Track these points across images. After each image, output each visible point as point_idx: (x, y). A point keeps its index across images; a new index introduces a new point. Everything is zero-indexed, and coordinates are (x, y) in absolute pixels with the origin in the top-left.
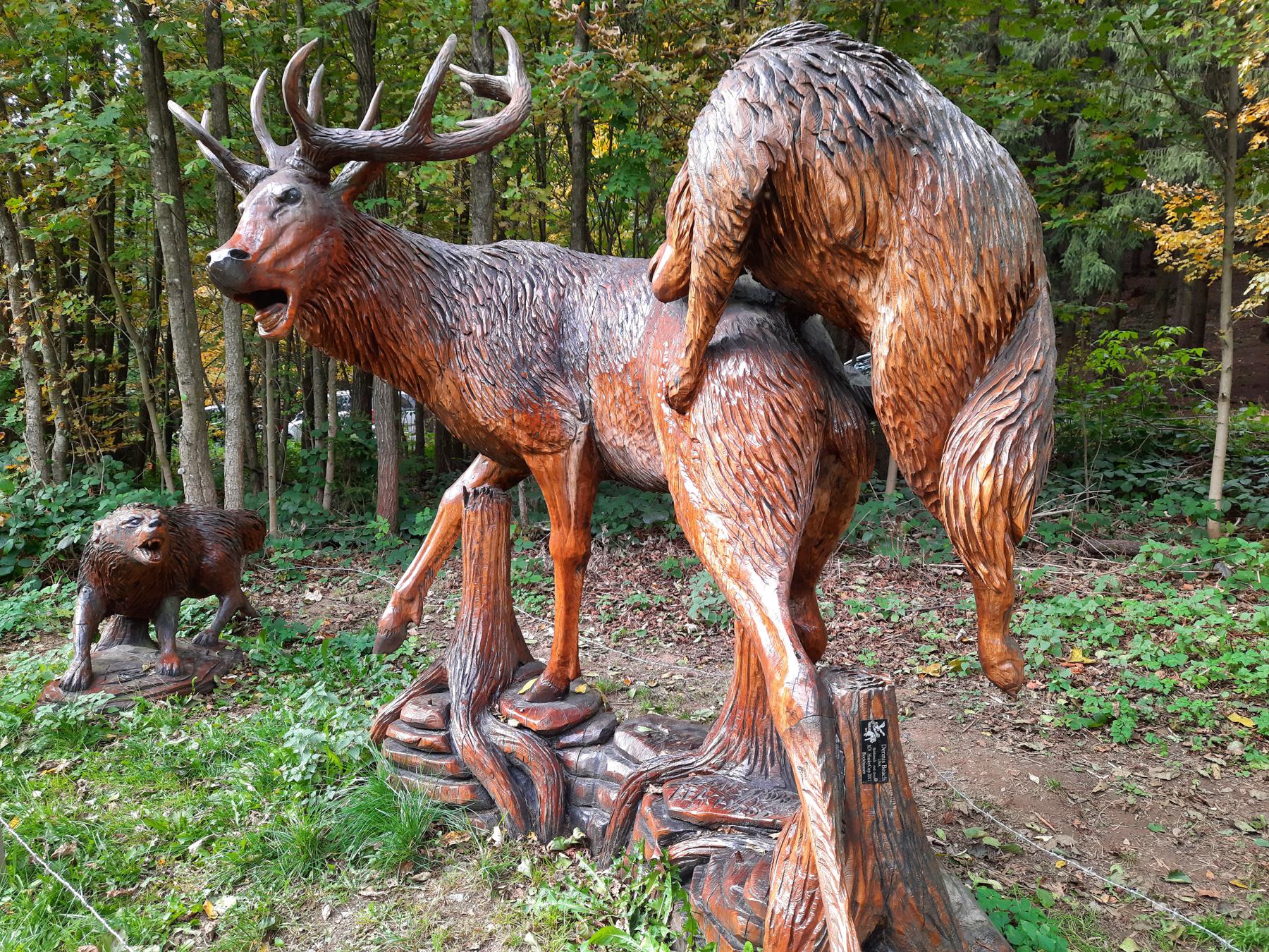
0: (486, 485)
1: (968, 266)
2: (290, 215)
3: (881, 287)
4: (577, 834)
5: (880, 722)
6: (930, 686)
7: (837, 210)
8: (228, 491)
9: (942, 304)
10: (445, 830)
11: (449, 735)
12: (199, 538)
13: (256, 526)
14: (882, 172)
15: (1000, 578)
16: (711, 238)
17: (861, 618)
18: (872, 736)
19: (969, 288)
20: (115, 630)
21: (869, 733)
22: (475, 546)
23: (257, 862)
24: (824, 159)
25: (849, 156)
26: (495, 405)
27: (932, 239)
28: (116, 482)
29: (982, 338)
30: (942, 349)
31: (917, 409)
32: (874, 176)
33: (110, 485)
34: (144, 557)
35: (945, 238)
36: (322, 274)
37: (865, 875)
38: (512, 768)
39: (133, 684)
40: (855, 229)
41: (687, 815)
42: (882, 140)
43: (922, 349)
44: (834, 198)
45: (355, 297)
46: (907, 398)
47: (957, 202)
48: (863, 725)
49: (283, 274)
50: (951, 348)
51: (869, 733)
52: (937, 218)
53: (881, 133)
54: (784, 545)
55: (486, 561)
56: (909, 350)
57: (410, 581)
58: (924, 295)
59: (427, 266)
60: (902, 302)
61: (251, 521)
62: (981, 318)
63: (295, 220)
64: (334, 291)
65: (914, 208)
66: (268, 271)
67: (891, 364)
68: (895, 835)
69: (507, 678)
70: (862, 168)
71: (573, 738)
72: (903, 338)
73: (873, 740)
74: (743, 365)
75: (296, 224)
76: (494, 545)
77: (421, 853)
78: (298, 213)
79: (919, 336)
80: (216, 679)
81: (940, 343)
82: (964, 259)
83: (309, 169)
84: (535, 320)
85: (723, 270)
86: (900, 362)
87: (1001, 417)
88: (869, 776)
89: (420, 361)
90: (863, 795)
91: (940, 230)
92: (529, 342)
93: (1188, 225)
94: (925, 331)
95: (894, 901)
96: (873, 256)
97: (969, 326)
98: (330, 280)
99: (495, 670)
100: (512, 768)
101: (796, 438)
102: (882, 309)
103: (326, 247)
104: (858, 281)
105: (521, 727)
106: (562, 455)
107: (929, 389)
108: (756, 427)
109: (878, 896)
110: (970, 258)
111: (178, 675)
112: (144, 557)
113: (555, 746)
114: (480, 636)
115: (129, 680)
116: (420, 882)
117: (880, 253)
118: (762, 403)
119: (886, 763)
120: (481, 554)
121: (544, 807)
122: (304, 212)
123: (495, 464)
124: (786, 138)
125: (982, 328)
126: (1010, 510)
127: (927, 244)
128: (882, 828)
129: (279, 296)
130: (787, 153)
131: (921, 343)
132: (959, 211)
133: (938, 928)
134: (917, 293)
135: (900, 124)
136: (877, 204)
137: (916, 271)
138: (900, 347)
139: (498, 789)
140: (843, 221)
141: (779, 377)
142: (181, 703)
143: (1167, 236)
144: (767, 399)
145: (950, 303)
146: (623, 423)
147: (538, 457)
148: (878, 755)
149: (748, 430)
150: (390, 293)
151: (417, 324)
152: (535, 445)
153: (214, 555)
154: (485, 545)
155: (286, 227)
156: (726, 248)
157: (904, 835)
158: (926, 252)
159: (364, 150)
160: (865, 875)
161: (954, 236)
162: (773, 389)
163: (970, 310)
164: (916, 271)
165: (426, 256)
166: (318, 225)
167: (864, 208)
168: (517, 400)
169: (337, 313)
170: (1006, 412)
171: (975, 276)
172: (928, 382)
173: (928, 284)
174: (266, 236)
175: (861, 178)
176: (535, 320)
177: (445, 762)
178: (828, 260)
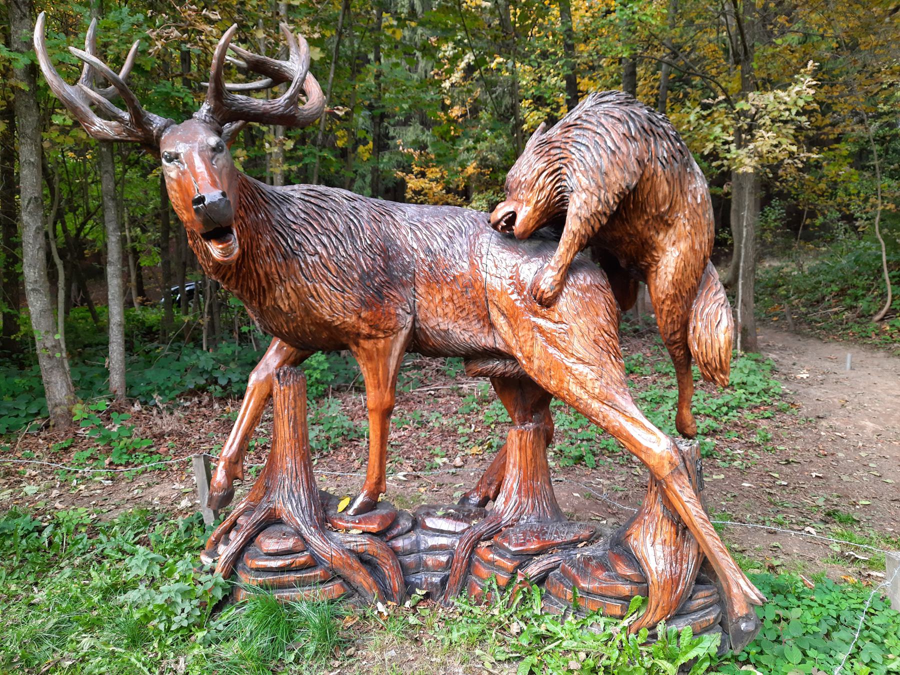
3: (670, 239)
4: (420, 592)
16: (597, 207)
22: (292, 412)
26: (344, 307)
38: (365, 560)
41: (527, 550)
60: (683, 246)
67: (676, 277)
71: (395, 532)
72: (683, 264)
74: (589, 279)
85: (597, 226)
86: (680, 276)
89: (266, 274)
92: (369, 261)
93: (423, 175)
96: (670, 222)
100: (365, 560)
102: (670, 249)
118: (603, 299)
121: (396, 583)
123: (292, 349)
139: (361, 578)
143: (412, 181)
146: (450, 315)
147: (372, 341)
152: (374, 333)
156: (605, 214)
168: (362, 302)
178: (650, 222)
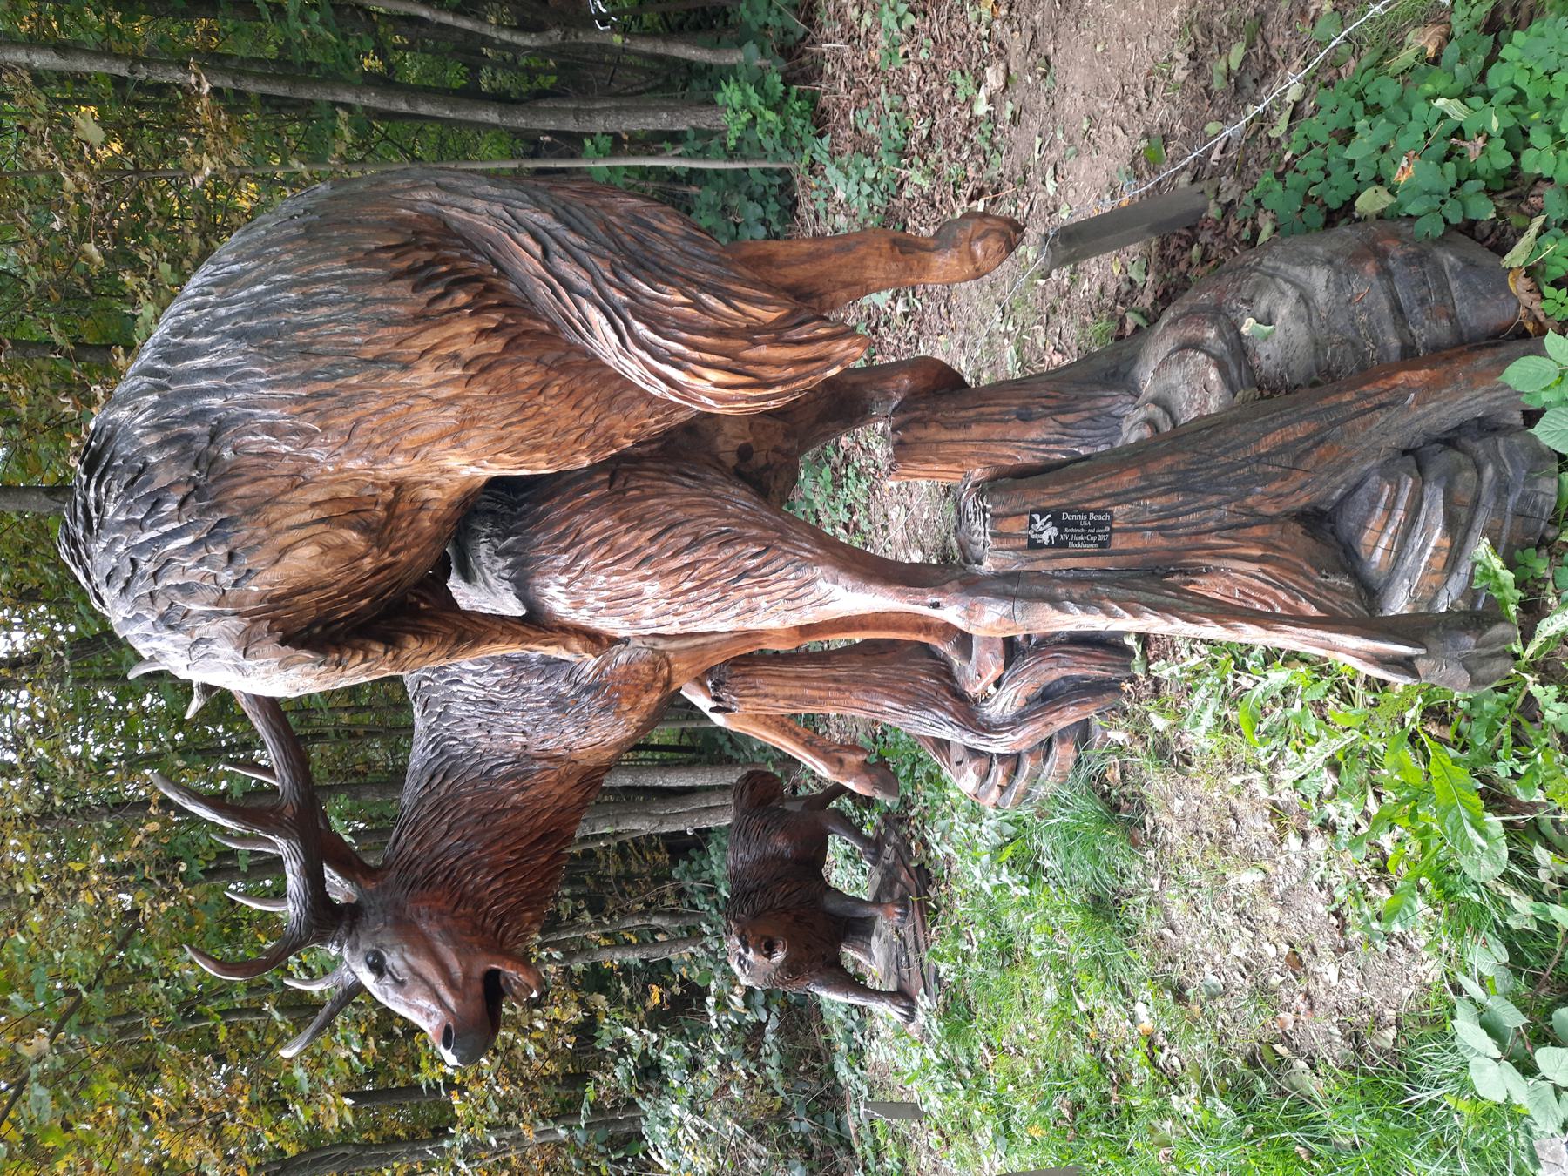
0: (709, 684)
1: (393, 376)
2: (399, 964)
5: (1032, 521)
6: (1010, 8)
7: (329, 558)
8: (714, 782)
9: (451, 412)
10: (1103, 780)
11: (999, 755)
12: (763, 861)
13: (752, 788)
14: (267, 502)
15: (849, 347)
17: (906, 55)
18: (1049, 533)
19: (425, 375)
20: (855, 948)
21: (1045, 538)
22: (781, 703)
23: (1105, 970)
24: (258, 579)
25: (249, 551)
27: (357, 432)
28: (702, 870)
29: (497, 344)
30: (518, 406)
31: (605, 422)
32: (274, 514)
33: (706, 876)
34: (779, 957)
35: (352, 416)
36: (462, 922)
37: (1228, 547)
39: (912, 957)
40: (353, 528)
42: (219, 506)
43: (519, 431)
44: (312, 564)
45: (488, 874)
46: (590, 437)
47: (298, 401)
48: (1034, 545)
49: (467, 976)
50: (518, 393)
51: (1045, 538)
52: (324, 428)
53: (209, 508)
54: (790, 568)
55: (800, 692)
56: (522, 447)
57: (820, 764)
58: (441, 437)
59: (445, 778)
61: (746, 794)
62: (468, 350)
63: (403, 958)
64: (482, 901)
65: (313, 455)
66: (464, 999)
68: (1184, 504)
69: (939, 672)
70: (262, 532)
72: (506, 457)
73: (1054, 532)
75: (407, 956)
76: (780, 681)
77: (1121, 812)
78: (395, 954)
79: (500, 439)
80: (915, 865)
81: (509, 410)
82: (382, 387)
83: (341, 933)
84: (503, 687)
87: (614, 338)
88: (1101, 538)
90: (1124, 547)
91: (343, 422)
94: (493, 431)
95: (1270, 509)
96: (389, 495)
97: (481, 367)
98: (469, 909)
99: (929, 687)
100: (1048, 698)
101: (650, 534)
103: (431, 918)
104: (427, 501)
105: (997, 684)
106: (672, 656)
107: (577, 412)
108: (635, 586)
109: (1258, 531)
110: (381, 375)
111: (906, 908)
112: (779, 957)
113: (1025, 645)
114: (888, 703)
115: (908, 960)
116: (1155, 830)
117: (384, 488)
118: (602, 578)
119: (1087, 512)
120: (790, 698)
122: (392, 947)
124: (234, 624)
125: (483, 346)
126: (752, 334)
127: (364, 440)
128: (1172, 521)
129: (492, 977)
130: (254, 622)
131: (511, 433)
132: (311, 396)
133: (1317, 445)
134: (438, 447)
135: (191, 479)
136: (314, 505)
137: (406, 451)
138: (518, 459)
139: (1070, 715)
140: (345, 545)
141: (565, 550)
142: (936, 912)
144: (596, 570)
145: (450, 402)
148: (1076, 524)
149: (639, 594)
150: (481, 827)
151: (518, 791)
152: (660, 684)
153: (780, 844)
154: (780, 693)
155: (410, 968)
157: (1187, 489)
158: (378, 440)
159: (311, 881)
160: (1228, 547)
161: (347, 403)
162: (583, 563)
163: (457, 372)
164: (406, 451)
165: (432, 777)
166: (406, 930)
167: (322, 521)
169: (508, 895)
170: (608, 330)
171: (406, 367)
172: (564, 414)
173: (425, 433)
174: (428, 997)
175: (279, 532)
176: (503, 687)
177: (1027, 765)
